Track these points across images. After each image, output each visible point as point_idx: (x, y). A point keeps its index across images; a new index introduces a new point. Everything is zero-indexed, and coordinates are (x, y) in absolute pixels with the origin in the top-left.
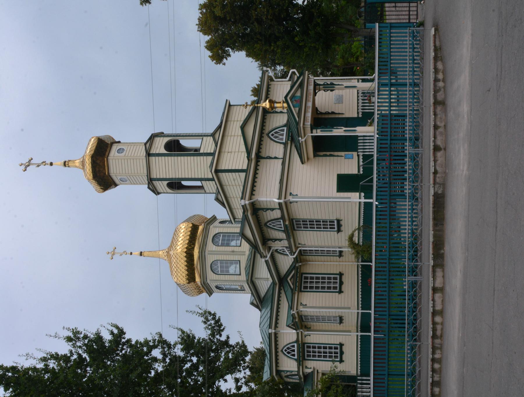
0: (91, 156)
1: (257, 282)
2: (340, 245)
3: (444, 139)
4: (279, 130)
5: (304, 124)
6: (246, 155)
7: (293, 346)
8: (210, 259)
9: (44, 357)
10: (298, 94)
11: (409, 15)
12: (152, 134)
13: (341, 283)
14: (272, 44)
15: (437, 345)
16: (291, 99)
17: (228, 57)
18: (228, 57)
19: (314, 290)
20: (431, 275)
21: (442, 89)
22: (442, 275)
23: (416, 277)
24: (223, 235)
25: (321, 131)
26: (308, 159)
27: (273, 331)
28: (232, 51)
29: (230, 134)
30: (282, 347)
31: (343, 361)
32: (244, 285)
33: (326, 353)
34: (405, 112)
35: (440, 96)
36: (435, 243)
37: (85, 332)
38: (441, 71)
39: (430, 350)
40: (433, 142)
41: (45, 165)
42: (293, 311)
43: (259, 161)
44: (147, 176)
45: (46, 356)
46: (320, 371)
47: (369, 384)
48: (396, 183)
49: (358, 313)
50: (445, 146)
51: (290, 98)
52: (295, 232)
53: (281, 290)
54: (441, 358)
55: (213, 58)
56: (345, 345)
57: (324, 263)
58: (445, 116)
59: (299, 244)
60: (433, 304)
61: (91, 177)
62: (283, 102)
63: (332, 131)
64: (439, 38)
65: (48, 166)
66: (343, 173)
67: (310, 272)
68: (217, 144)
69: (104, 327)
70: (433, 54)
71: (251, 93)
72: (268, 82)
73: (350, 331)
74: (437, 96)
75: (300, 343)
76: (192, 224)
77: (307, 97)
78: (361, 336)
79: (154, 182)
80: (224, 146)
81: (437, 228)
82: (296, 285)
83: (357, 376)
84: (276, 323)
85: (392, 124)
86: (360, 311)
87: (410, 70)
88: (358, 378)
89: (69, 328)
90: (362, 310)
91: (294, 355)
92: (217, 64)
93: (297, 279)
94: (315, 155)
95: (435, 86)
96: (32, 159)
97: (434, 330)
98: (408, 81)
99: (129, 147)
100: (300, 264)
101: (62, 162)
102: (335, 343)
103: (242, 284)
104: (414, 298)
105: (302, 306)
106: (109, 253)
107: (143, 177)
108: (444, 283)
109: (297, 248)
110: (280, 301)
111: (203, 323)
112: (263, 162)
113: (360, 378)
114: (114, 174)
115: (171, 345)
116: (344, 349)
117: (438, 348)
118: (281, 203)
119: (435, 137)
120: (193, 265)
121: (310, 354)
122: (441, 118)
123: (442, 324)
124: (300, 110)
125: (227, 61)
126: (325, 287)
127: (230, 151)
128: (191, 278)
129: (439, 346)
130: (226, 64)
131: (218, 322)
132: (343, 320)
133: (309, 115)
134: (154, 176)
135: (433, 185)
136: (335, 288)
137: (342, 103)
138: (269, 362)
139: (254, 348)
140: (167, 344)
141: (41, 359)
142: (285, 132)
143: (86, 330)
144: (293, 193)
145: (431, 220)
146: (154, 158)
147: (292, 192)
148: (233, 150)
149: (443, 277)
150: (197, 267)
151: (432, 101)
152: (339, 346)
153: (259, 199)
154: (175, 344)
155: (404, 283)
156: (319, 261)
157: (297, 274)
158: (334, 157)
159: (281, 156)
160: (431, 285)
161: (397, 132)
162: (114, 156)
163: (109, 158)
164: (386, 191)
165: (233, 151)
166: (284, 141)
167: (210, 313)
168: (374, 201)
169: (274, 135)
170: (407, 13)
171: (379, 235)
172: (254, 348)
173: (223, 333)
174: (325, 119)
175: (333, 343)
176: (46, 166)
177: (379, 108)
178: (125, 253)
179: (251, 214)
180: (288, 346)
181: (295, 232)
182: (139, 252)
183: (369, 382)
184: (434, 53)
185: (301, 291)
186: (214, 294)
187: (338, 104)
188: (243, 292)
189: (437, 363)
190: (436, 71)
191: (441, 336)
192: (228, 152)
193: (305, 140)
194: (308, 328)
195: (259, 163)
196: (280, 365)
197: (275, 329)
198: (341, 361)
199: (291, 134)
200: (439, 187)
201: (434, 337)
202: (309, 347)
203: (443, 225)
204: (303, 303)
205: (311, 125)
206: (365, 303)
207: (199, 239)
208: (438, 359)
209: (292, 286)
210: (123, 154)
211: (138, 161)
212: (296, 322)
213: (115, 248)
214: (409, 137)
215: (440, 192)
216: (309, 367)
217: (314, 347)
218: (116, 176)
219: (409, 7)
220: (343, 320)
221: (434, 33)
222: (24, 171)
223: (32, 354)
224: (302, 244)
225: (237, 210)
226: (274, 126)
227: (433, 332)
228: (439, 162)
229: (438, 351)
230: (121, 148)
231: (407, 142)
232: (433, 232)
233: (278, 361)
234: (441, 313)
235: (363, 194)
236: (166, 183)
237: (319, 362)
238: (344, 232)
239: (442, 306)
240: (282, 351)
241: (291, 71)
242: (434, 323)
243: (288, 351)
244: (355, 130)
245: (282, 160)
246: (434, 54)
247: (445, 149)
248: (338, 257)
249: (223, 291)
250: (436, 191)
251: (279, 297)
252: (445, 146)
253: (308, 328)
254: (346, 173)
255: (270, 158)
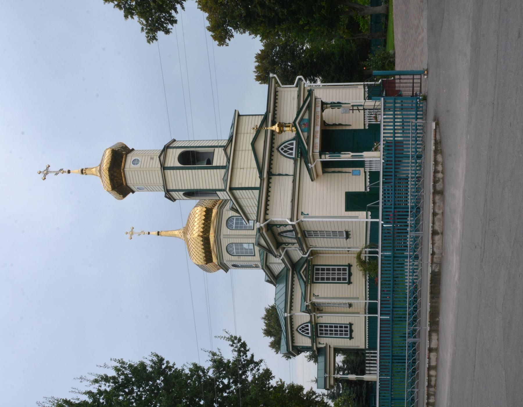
0: (108, 169)
1: (271, 266)
2: (349, 246)
3: (441, 225)
4: (305, 326)
5: (313, 152)
6: (258, 175)
7: (307, 326)
8: (225, 243)
9: (96, 379)
10: (306, 117)
11: (413, 83)
12: (165, 146)
13: (350, 274)
14: (276, 26)
15: (431, 393)
16: (299, 124)
17: (231, 38)
18: (231, 38)
19: (325, 281)
20: (427, 339)
21: (441, 180)
22: (437, 338)
23: (415, 339)
24: (236, 218)
25: (329, 156)
26: (317, 176)
27: (289, 315)
28: (235, 31)
29: (241, 149)
30: (297, 327)
31: (353, 338)
32: (259, 264)
33: (337, 331)
34: (408, 153)
35: (439, 186)
36: (431, 312)
37: (130, 362)
38: (441, 163)
39: (426, 396)
40: (432, 227)
41: (63, 173)
42: (307, 303)
43: (271, 178)
44: (164, 186)
45: (97, 378)
46: (332, 346)
47: (376, 357)
48: (401, 183)
49: (366, 303)
50: (443, 231)
51: (298, 123)
52: (306, 239)
53: (294, 274)
54: (434, 402)
55: (215, 38)
56: (354, 324)
57: (334, 255)
58: (443, 204)
59: (310, 246)
60: (429, 361)
61: (110, 189)
62: (292, 127)
63: (339, 156)
64: (440, 132)
65: (66, 174)
66: (350, 190)
67: (322, 264)
68: (229, 160)
69: (146, 358)
70: (433, 147)
71: (255, 60)
72: (275, 88)
73: (358, 313)
74: (436, 186)
75: (313, 324)
76: (206, 208)
77: (315, 120)
78: (369, 317)
79: (171, 193)
80: (236, 162)
81: (434, 301)
82: (308, 278)
83: (365, 349)
84: (291, 306)
85: (396, 186)
86: (368, 301)
87: (412, 173)
88: (367, 351)
89: (116, 359)
90: (369, 300)
91: (308, 333)
92: (220, 46)
93: (309, 277)
94: (324, 172)
95: (434, 177)
96: (49, 166)
97: (429, 381)
98: (410, 153)
99: (144, 157)
100: (312, 257)
101: (79, 170)
102: (345, 323)
103: (256, 263)
104: (414, 312)
105: (314, 297)
106: (127, 233)
107: (160, 187)
108: (438, 345)
109: (308, 249)
110: (294, 284)
111: (230, 346)
112: (275, 179)
113: (368, 351)
114: (132, 185)
115: (204, 369)
116: (353, 327)
117: (432, 395)
118: (294, 225)
119: (433, 223)
120: (210, 247)
121: (319, 272)
122: (439, 206)
123: (436, 376)
124: (309, 137)
125: (231, 42)
126: (335, 278)
127: (242, 167)
128: (208, 259)
129: (433, 393)
130: (229, 45)
131: (244, 345)
132: (350, 235)
133: (318, 129)
134: (170, 187)
135: (431, 265)
136: (344, 279)
137: (349, 113)
138: (286, 340)
139: (269, 306)
140: (201, 369)
141: (93, 381)
142: (294, 146)
143: (130, 361)
144: (304, 213)
145: (428, 293)
146: (169, 171)
147: (303, 211)
148: (245, 167)
149: (438, 340)
150: (213, 249)
151: (432, 191)
152: (348, 326)
153: (273, 219)
154: (209, 369)
155: (406, 281)
156: (329, 254)
157: (309, 268)
158: (342, 174)
159: (291, 172)
160: (428, 346)
161: (401, 194)
162: (130, 168)
163: (125, 169)
164: (389, 337)
165: (245, 167)
166: (294, 156)
167: (236, 338)
168: (380, 220)
169: (284, 149)
170: (411, 81)
171: (384, 247)
172: (269, 306)
173: (248, 353)
174: (333, 131)
175: (343, 323)
176: (64, 173)
177: (385, 127)
178: (143, 233)
179: (265, 232)
180: (303, 326)
181: (306, 239)
182: (157, 232)
183: (376, 355)
184: (434, 146)
185: (313, 283)
186: (229, 270)
187: (345, 114)
188: (258, 268)
189: (431, 406)
190: (436, 163)
191: (435, 386)
192: (241, 169)
193: (315, 166)
194: (320, 310)
195: (271, 181)
196: (295, 341)
197: (290, 313)
198: (351, 338)
199: (301, 150)
200: (436, 266)
201: (429, 386)
202: (321, 326)
203: (439, 297)
204: (315, 294)
205: (320, 152)
206: (372, 294)
207: (213, 223)
208: (432, 403)
209: (305, 279)
210: (138, 166)
211: (153, 172)
212: (309, 309)
213: (133, 228)
214: (411, 205)
215: (437, 270)
216: (322, 343)
217: (326, 327)
218: (133, 186)
219: (413, 79)
220: (350, 235)
221: (434, 128)
222: (44, 180)
223: (85, 376)
224: (313, 246)
225: (251, 215)
226: (283, 141)
227: (428, 382)
228: (436, 245)
229: (432, 397)
230: (136, 159)
231: (408, 228)
232: (430, 304)
233: (293, 323)
234: (435, 368)
235: (369, 213)
236: (181, 193)
237: (330, 339)
238: (352, 238)
239: (436, 362)
240: (297, 330)
241: (298, 77)
242: (429, 376)
243: (285, 149)
244: (362, 156)
245: (292, 176)
246: (434, 148)
247: (442, 234)
248: (348, 339)
249: (239, 268)
250: (433, 269)
251: (293, 281)
252: (443, 231)
253: (320, 310)
254: (354, 190)
255: (280, 175)
